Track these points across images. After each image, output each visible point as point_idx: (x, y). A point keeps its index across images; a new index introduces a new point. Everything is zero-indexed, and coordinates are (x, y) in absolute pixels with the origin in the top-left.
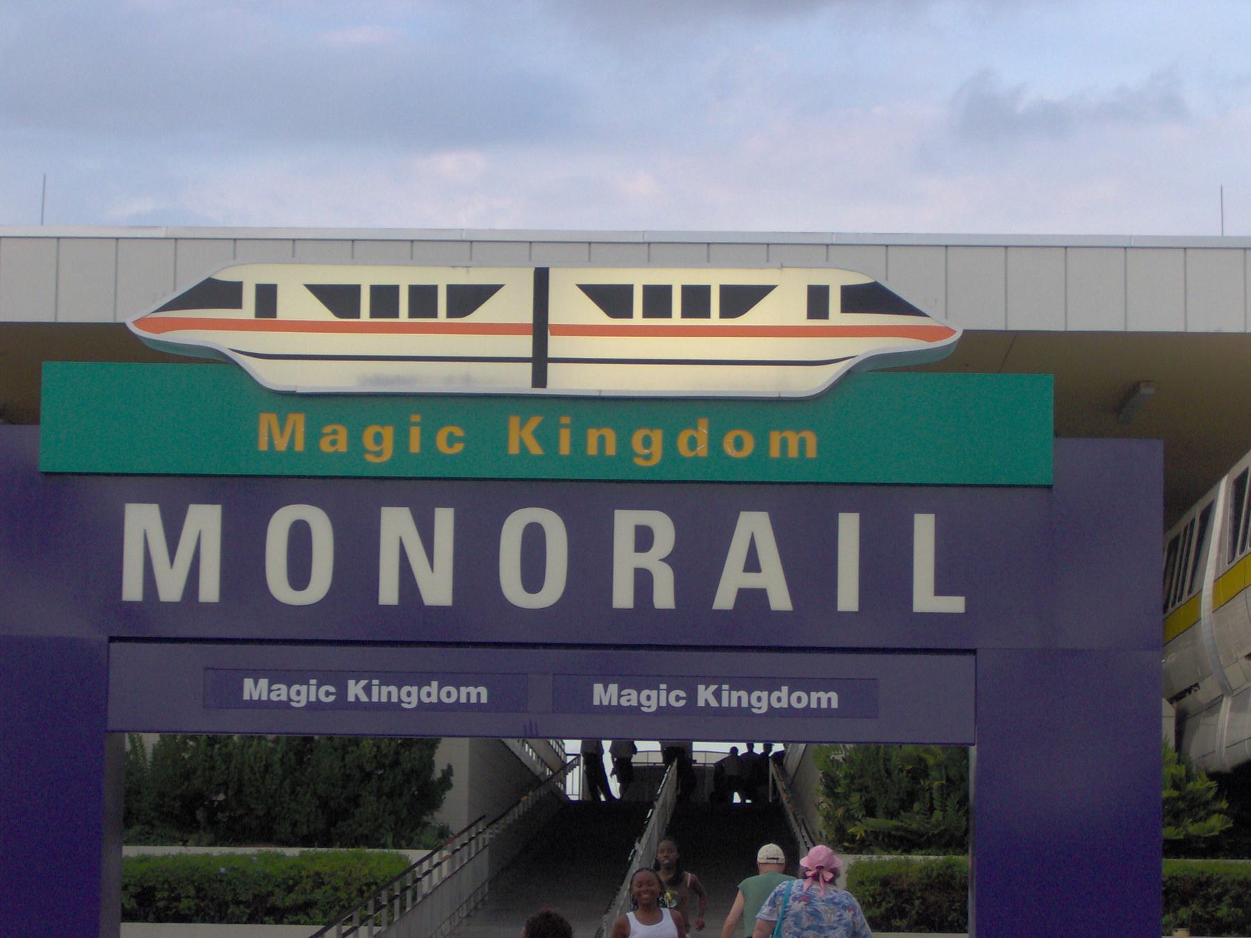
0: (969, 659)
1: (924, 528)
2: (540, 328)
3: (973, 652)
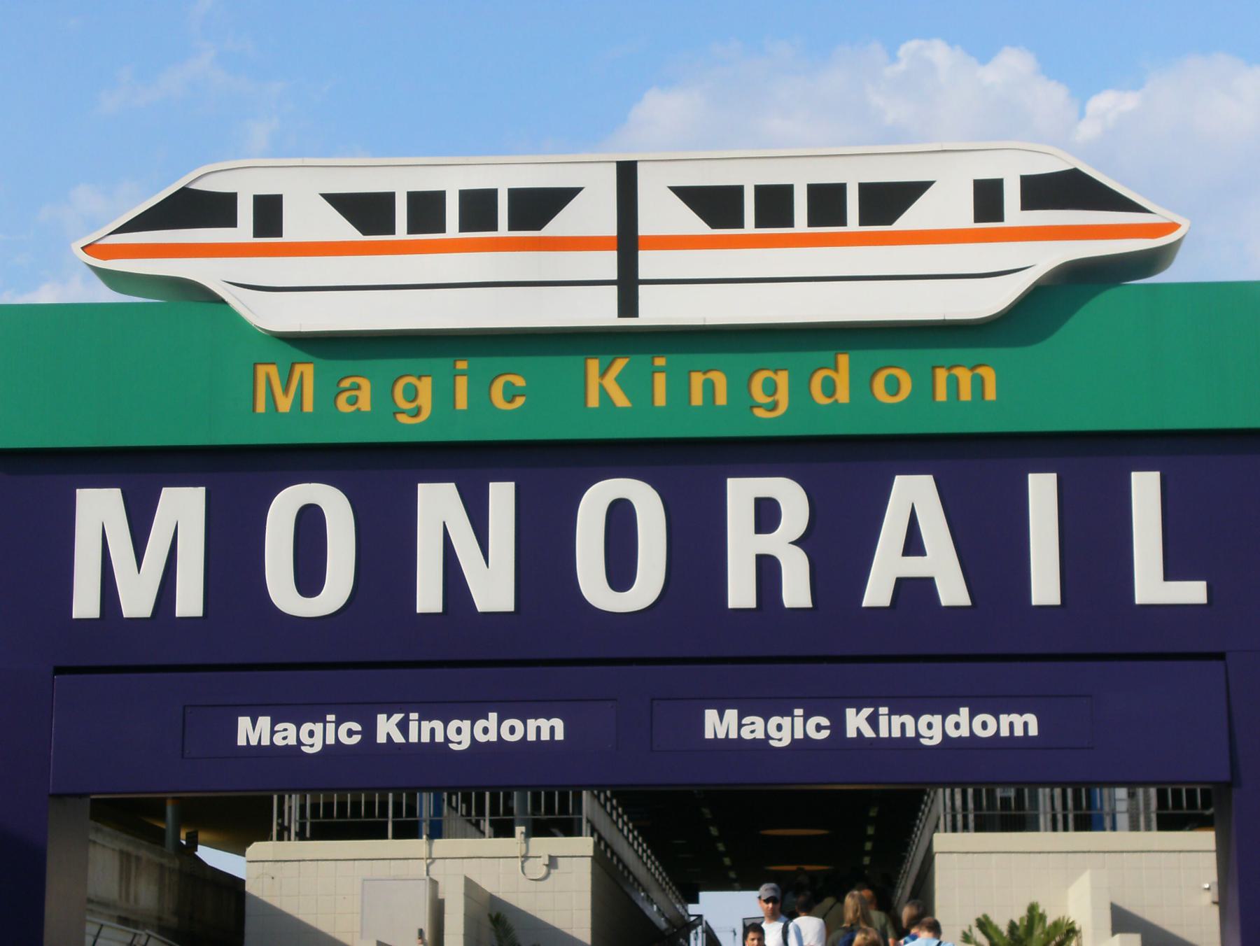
0: (1217, 665)
1: (1145, 489)
2: (628, 242)
3: (1220, 656)
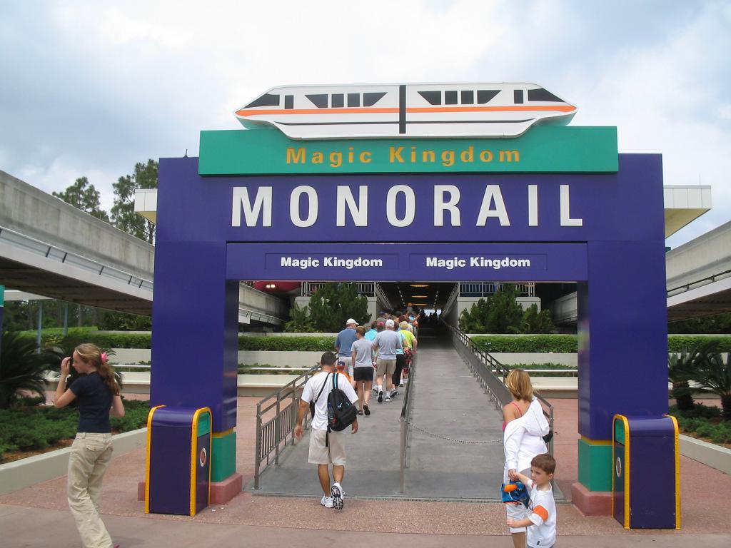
1: (564, 191)
2: (402, 110)
3: (586, 242)
